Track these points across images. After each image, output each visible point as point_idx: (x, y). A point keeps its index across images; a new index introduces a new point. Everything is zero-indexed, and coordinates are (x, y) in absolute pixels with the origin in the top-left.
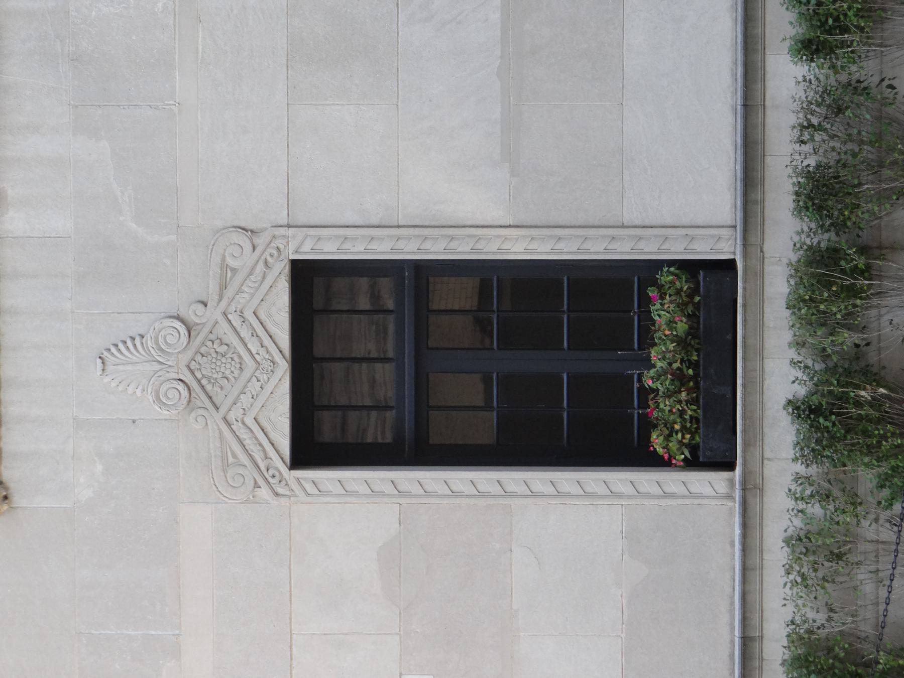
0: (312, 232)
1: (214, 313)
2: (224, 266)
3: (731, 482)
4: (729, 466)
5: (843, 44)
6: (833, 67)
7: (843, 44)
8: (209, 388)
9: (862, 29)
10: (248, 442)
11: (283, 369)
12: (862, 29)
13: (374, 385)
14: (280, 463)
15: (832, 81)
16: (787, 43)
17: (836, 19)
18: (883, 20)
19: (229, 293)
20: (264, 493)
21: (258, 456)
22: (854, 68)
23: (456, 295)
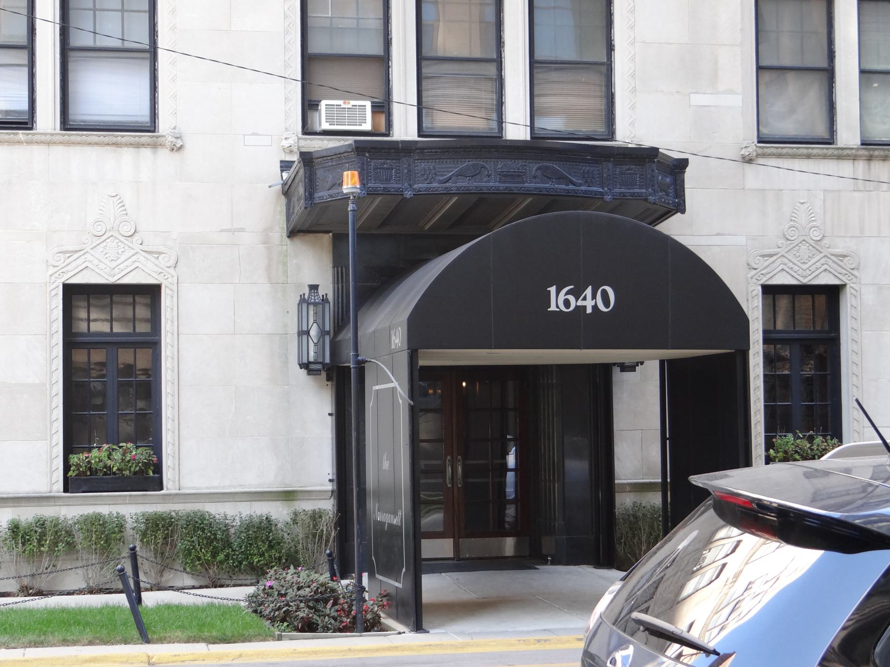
0: (175, 294)
1: (138, 248)
2: (160, 253)
3: (58, 492)
4: (66, 490)
5: (17, 544)
6: (6, 540)
7: (17, 544)
8: (102, 245)
9: (24, 552)
10: (126, 263)
11: (793, 282)
12: (24, 552)
13: (98, 322)
14: (764, 281)
15: (232, 531)
16: (17, 517)
17: (29, 540)
18: (28, 562)
19: (833, 258)
20: (52, 270)
21: (121, 267)
22: (5, 549)
23: (142, 360)
